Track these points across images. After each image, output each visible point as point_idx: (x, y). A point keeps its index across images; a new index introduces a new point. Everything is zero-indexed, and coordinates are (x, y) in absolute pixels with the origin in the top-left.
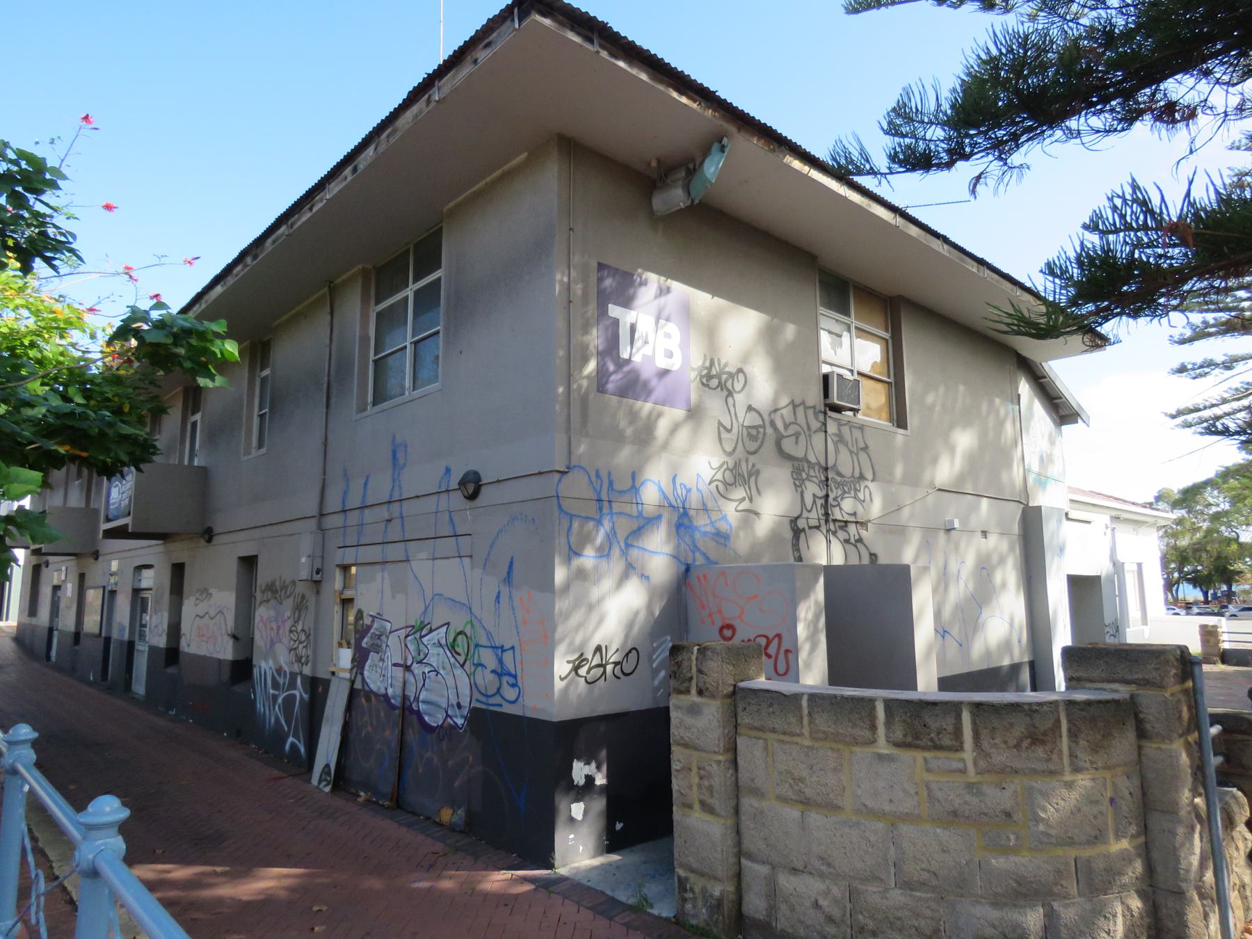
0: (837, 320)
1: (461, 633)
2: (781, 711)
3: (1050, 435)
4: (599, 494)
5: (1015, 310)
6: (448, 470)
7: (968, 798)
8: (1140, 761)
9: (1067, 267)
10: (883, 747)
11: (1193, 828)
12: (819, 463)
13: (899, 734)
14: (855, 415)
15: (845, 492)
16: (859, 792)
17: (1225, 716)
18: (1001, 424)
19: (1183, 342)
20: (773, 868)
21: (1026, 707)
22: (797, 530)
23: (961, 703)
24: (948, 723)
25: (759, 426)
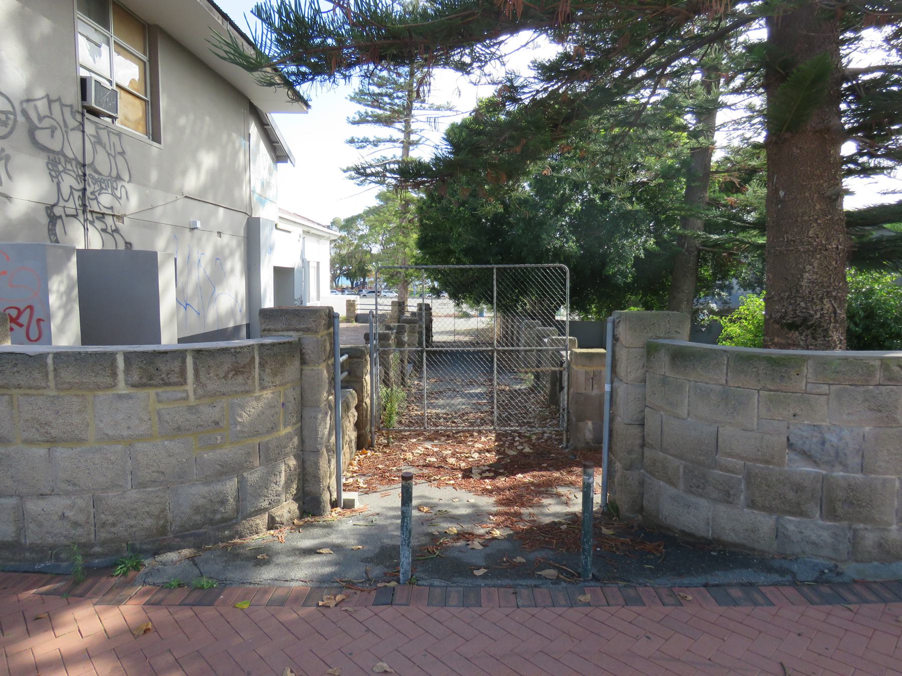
0: (96, 29)
2: (26, 370)
3: (270, 168)
5: (232, 41)
7: (189, 416)
8: (301, 378)
9: (270, 14)
10: (122, 388)
11: (327, 414)
12: (76, 159)
13: (136, 378)
14: (113, 122)
15: (102, 188)
16: (102, 425)
17: (351, 349)
18: (235, 154)
19: (354, 123)
20: (21, 498)
21: (233, 350)
23: (186, 351)
24: (176, 365)
25: (9, 112)
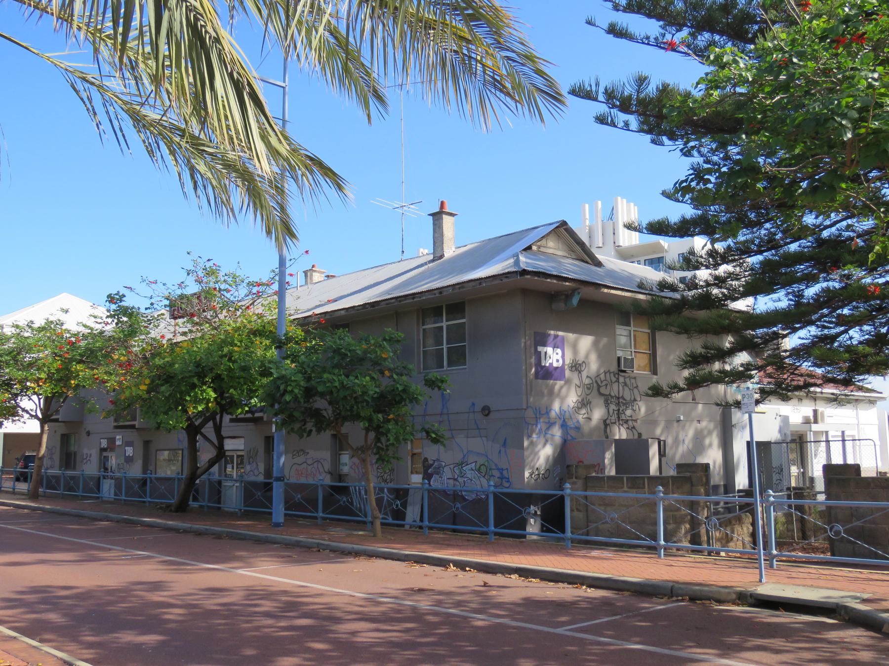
1: (483, 465)
4: (536, 415)
6: (473, 404)
10: (625, 489)
12: (615, 396)
13: (629, 485)
22: (606, 424)
